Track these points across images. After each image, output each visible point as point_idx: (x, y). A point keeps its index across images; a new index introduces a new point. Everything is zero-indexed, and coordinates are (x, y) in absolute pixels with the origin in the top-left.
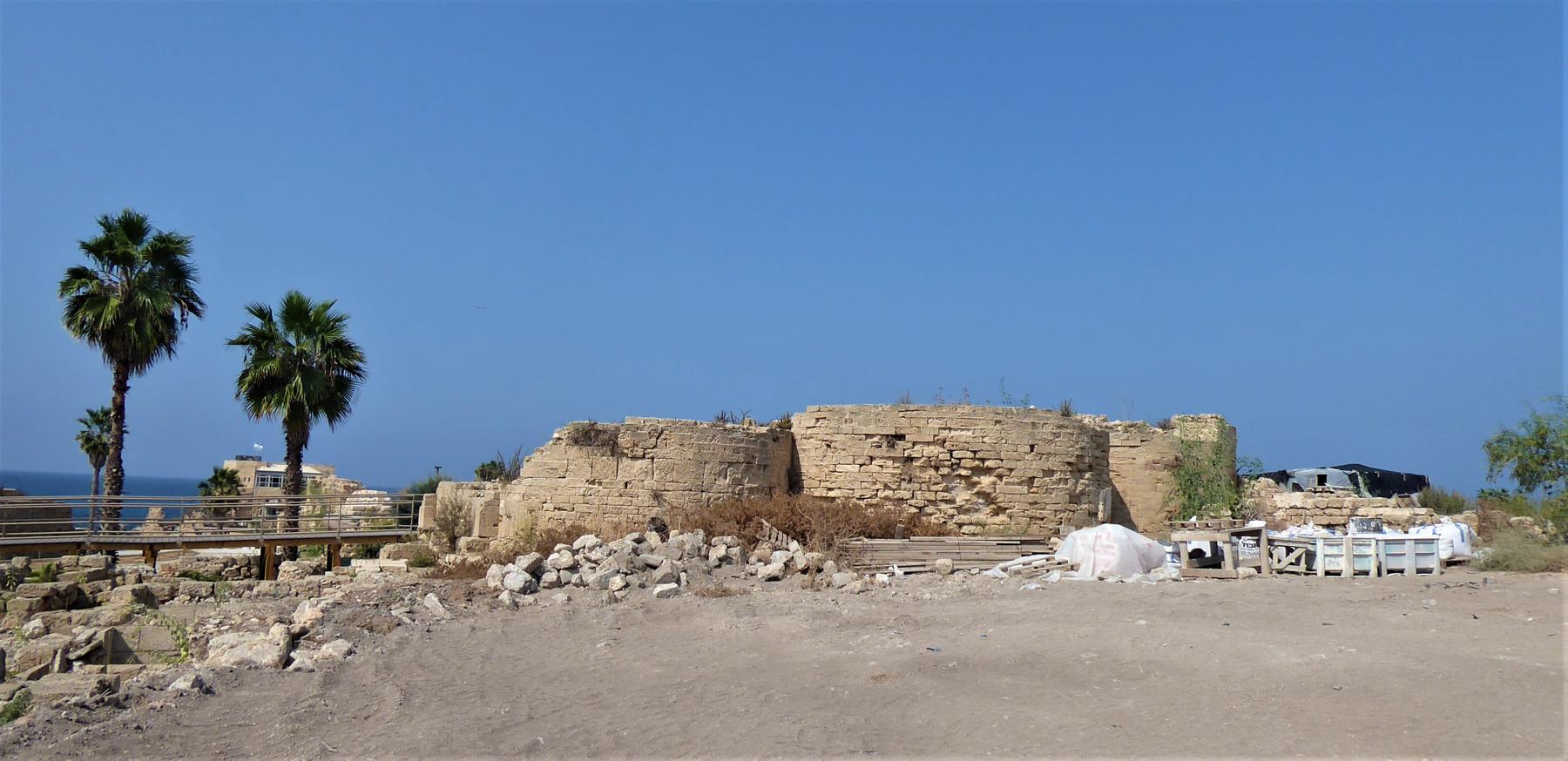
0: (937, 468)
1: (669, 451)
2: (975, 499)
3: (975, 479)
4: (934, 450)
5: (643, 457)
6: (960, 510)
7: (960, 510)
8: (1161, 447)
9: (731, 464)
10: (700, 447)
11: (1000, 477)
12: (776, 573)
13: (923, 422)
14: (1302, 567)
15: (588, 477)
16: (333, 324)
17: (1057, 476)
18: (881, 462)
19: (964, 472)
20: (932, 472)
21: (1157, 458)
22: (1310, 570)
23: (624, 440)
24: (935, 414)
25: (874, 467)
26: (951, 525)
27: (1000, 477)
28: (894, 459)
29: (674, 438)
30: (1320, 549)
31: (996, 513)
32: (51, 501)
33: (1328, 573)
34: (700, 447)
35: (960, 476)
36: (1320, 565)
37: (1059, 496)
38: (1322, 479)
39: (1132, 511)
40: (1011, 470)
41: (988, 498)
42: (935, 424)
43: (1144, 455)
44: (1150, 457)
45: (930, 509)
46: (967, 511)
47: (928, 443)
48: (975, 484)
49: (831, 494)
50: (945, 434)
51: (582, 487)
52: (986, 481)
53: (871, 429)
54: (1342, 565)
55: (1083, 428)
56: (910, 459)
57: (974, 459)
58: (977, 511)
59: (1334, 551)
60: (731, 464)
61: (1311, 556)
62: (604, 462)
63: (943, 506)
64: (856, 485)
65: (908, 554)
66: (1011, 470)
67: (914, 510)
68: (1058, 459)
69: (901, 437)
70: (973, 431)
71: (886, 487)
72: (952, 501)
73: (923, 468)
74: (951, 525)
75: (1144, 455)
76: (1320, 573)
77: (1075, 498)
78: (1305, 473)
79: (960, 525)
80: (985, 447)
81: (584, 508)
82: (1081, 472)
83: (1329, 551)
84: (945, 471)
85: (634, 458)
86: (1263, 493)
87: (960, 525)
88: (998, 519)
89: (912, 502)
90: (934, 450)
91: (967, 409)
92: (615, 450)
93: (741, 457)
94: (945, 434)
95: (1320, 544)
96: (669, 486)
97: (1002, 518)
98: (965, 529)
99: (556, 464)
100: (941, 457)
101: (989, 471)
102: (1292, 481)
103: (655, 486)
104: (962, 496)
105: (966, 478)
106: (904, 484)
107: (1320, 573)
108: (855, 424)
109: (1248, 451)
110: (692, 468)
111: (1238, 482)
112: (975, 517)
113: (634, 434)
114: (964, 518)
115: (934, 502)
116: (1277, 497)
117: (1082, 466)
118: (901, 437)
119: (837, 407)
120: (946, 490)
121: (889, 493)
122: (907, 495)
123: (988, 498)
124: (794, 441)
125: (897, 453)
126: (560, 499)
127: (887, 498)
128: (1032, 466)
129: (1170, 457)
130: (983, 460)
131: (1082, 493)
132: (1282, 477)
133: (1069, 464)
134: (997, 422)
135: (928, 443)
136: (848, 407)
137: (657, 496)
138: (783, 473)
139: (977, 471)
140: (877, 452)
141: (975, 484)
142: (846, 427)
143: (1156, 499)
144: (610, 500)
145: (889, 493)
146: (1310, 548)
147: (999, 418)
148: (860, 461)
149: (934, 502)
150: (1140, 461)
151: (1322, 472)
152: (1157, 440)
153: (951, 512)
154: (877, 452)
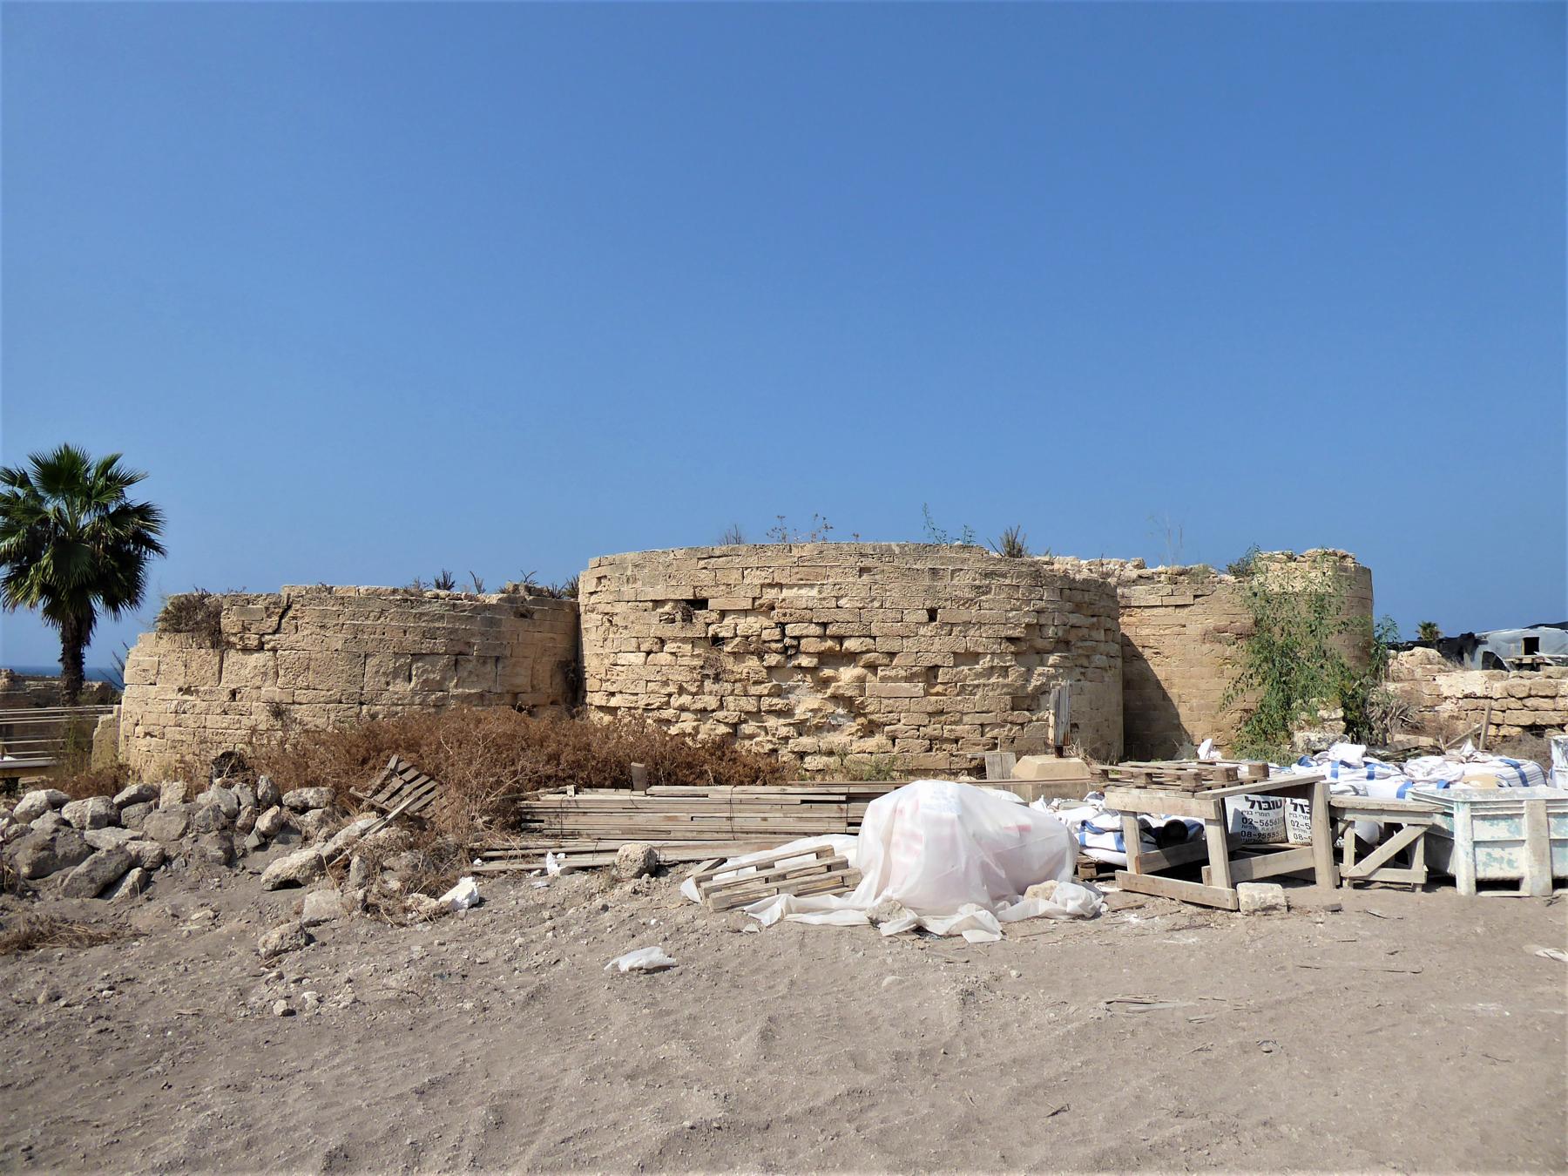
1: (300, 639)
2: (830, 708)
3: (827, 672)
5: (260, 647)
6: (801, 728)
7: (801, 728)
8: (1225, 606)
9: (417, 656)
10: (357, 630)
12: (292, 873)
13: (736, 575)
14: (1418, 871)
15: (181, 682)
16: (114, 481)
17: (985, 663)
19: (805, 661)
20: (753, 662)
21: (1223, 623)
22: (1439, 878)
24: (753, 561)
25: (664, 658)
26: (785, 755)
27: (872, 667)
28: (694, 642)
29: (310, 615)
30: (1461, 828)
31: (870, 729)
33: (1482, 885)
34: (357, 630)
35: (799, 667)
36: (1461, 865)
37: (990, 696)
38: (1531, 645)
39: (1183, 711)
40: (892, 655)
41: (853, 707)
42: (755, 578)
43: (1200, 620)
44: (1211, 623)
45: (747, 729)
46: (819, 729)
48: (826, 682)
49: (614, 702)
50: (770, 595)
54: (1521, 863)
55: (1038, 576)
56: (717, 641)
57: (823, 637)
58: (835, 728)
59: (1500, 831)
60: (417, 656)
61: (1438, 843)
63: (771, 722)
65: (640, 819)
66: (892, 655)
67: (722, 729)
68: (987, 631)
69: (702, 603)
71: (681, 690)
72: (786, 713)
74: (785, 755)
75: (1200, 620)
76: (1464, 885)
77: (1025, 701)
78: (1504, 638)
79: (801, 755)
80: (841, 616)
82: (1041, 654)
83: (1486, 831)
84: (772, 659)
85: (246, 650)
86: (1419, 673)
87: (801, 755)
88: (871, 743)
89: (720, 715)
92: (218, 641)
93: (440, 645)
94: (770, 595)
95: (1461, 816)
96: (301, 696)
97: (879, 739)
98: (811, 762)
100: (766, 635)
101: (851, 658)
102: (1482, 649)
104: (806, 702)
105: (812, 670)
106: (708, 685)
107: (1464, 885)
109: (1396, 610)
110: (341, 665)
111: (1374, 654)
112: (836, 739)
113: (243, 610)
114: (806, 742)
115: (757, 715)
116: (1441, 680)
117: (1040, 643)
118: (702, 603)
120: (778, 692)
121: (686, 699)
122: (712, 702)
124: (578, 616)
125: (697, 630)
126: (151, 719)
127: (683, 709)
128: (935, 646)
129: (1246, 620)
130: (840, 639)
131: (1042, 691)
132: (1458, 649)
133: (1010, 640)
134: (862, 571)
135: (745, 612)
136: (632, 556)
137: (278, 712)
138: (545, 667)
139: (825, 658)
141: (826, 682)
142: (628, 591)
143: (1218, 687)
145: (686, 699)
146: (1438, 820)
147: (867, 562)
148: (644, 647)
149: (757, 715)
150: (1195, 629)
151: (1532, 633)
152: (1221, 593)
153: (783, 731)
154: (668, 631)
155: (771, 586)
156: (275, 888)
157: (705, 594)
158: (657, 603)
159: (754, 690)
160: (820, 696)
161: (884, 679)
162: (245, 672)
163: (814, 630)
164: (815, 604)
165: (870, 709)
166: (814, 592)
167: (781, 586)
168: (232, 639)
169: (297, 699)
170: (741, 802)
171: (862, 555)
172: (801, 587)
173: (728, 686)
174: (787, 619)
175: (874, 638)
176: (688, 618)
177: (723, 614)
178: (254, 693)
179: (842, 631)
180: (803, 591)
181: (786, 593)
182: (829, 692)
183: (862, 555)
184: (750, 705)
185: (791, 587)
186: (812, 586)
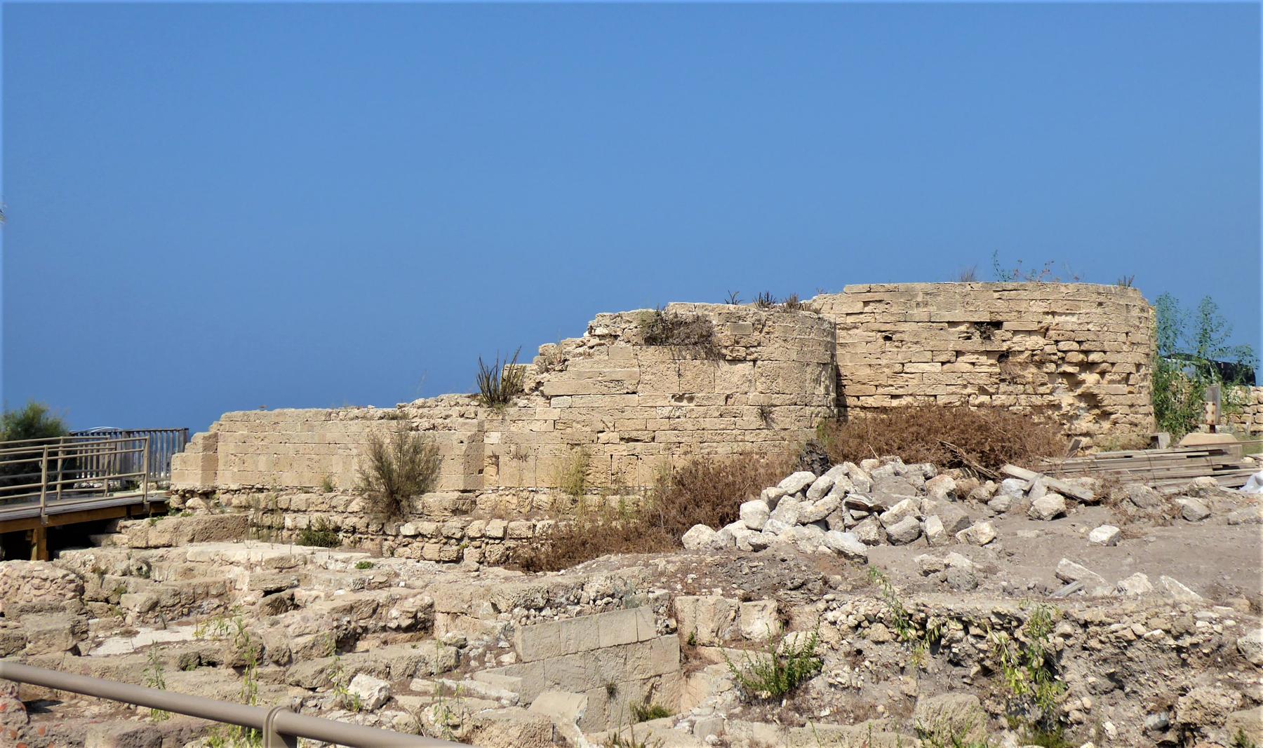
0: (1040, 364)
2: (1077, 403)
4: (1036, 341)
11: (1102, 374)
18: (973, 358)
19: (1070, 369)
23: (723, 336)
24: (1037, 295)
25: (962, 364)
27: (1102, 374)
28: (988, 353)
32: (25, 445)
40: (1113, 364)
42: (1039, 307)
47: (1030, 333)
51: (666, 406)
52: (1090, 378)
53: (957, 315)
62: (695, 368)
64: (939, 390)
69: (998, 325)
70: (1082, 314)
71: (983, 391)
73: (1024, 365)
80: (1091, 337)
81: (672, 436)
85: (735, 361)
90: (1036, 341)
91: (1072, 287)
97: (1106, 425)
99: (619, 373)
100: (1048, 349)
103: (763, 400)
106: (1003, 387)
108: (933, 309)
118: (998, 325)
119: (902, 286)
123: (1091, 400)
130: (1086, 352)
134: (1100, 304)
135: (1030, 333)
136: (919, 286)
139: (1088, 366)
140: (968, 345)
144: (707, 423)
145: (984, 399)
147: (1101, 299)
148: (944, 358)
154: (968, 345)
155: (1048, 313)
156: (1054, 518)
157: (1000, 318)
158: (952, 324)
159: (1042, 390)
160: (1071, 394)
161: (1111, 382)
162: (735, 379)
163: (1076, 346)
164: (1075, 327)
165: (1105, 403)
166: (1074, 319)
167: (1053, 313)
168: (724, 351)
169: (774, 402)
170: (1155, 459)
171: (1099, 294)
172: (1067, 314)
173: (1021, 387)
174: (1060, 338)
175: (1105, 352)
176: (987, 338)
177: (1015, 332)
178: (744, 398)
179: (1091, 348)
180: (1069, 318)
181: (1058, 319)
182: (1079, 391)
183: (1099, 294)
184: (1037, 401)
185: (1061, 314)
186: (1073, 314)
